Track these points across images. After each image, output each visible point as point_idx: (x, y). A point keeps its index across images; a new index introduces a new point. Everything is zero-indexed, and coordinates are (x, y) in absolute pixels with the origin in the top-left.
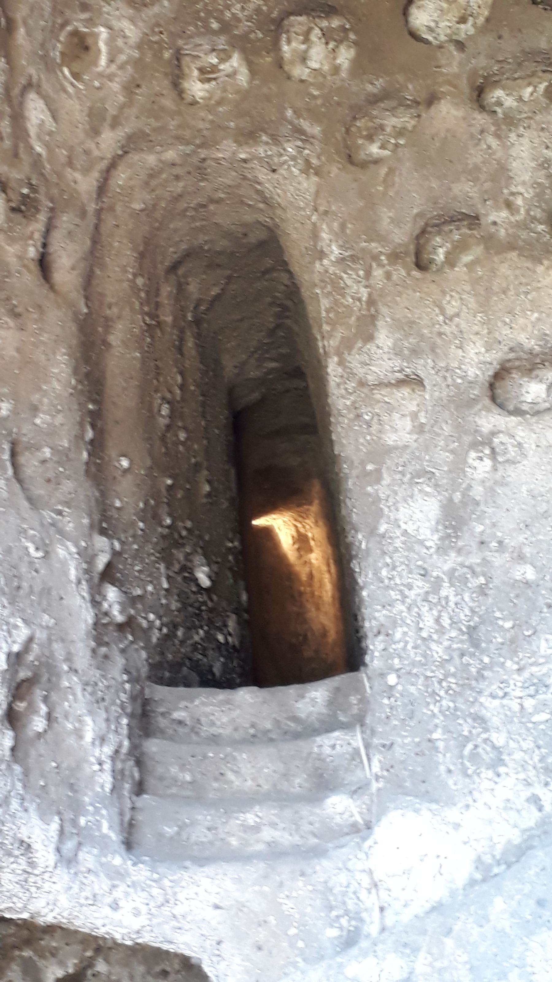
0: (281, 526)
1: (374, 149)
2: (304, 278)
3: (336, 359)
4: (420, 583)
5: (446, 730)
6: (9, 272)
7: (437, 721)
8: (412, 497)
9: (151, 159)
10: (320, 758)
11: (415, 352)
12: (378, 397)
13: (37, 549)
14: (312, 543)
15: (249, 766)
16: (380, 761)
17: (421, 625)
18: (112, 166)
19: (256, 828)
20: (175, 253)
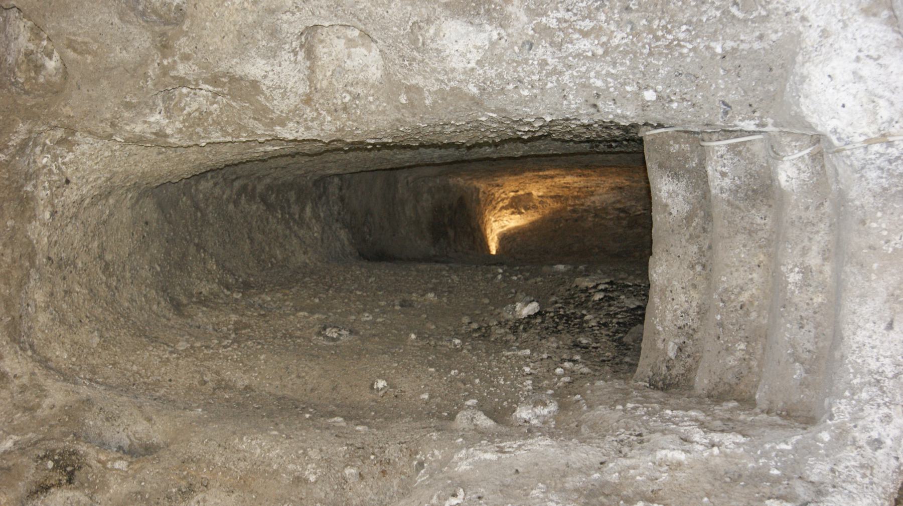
0: (499, 224)
1: (52, 64)
2: (194, 160)
3: (278, 128)
4: (541, 51)
5: (713, 36)
6: (137, 493)
7: (702, 46)
8: (438, 51)
9: (43, 318)
10: (735, 192)
11: (274, 32)
12: (325, 83)
13: (454, 495)
14: (521, 193)
15: (736, 274)
16: (742, 120)
17: (590, 54)
18: (44, 362)
19: (806, 271)
20: (159, 303)
